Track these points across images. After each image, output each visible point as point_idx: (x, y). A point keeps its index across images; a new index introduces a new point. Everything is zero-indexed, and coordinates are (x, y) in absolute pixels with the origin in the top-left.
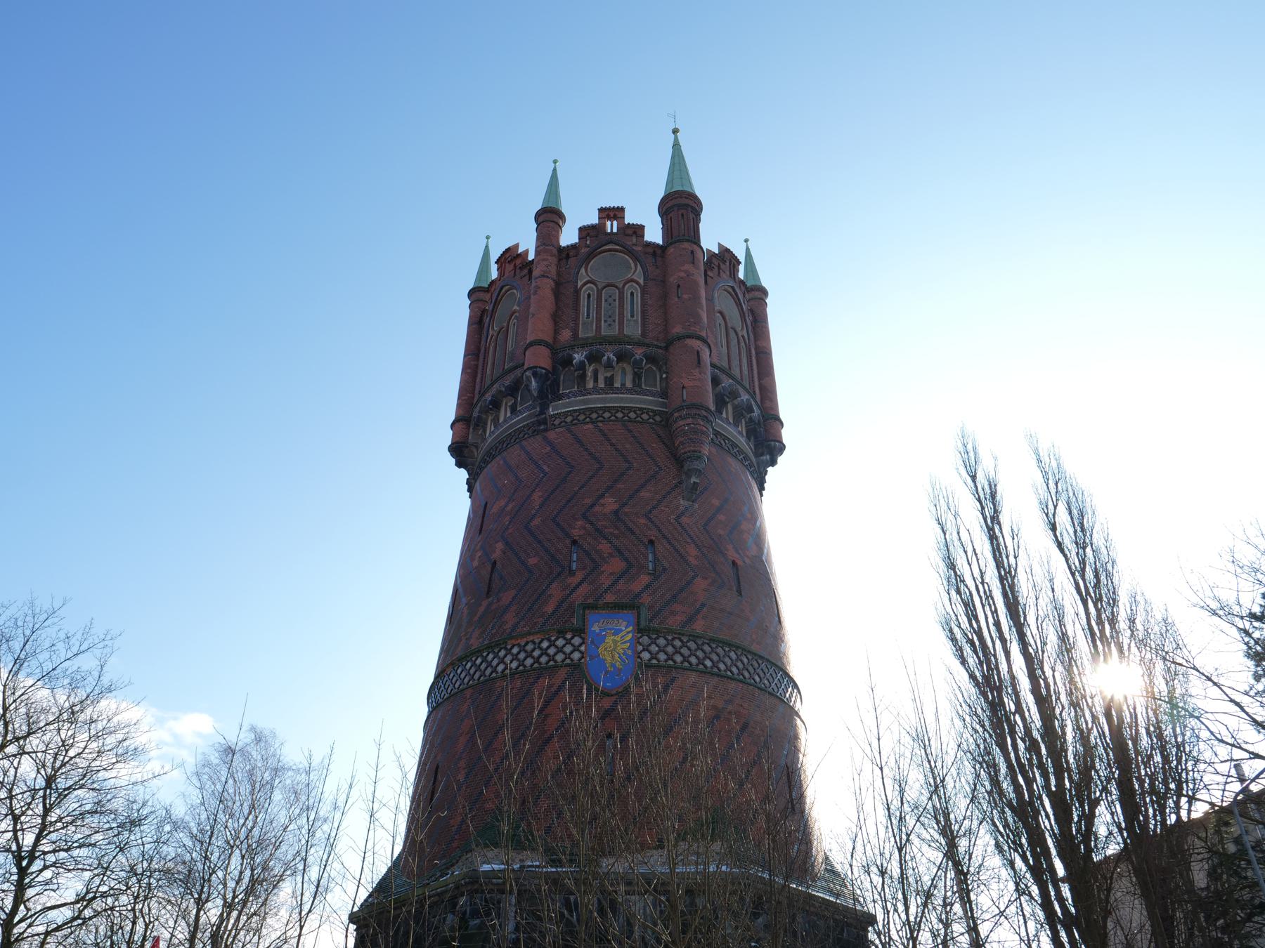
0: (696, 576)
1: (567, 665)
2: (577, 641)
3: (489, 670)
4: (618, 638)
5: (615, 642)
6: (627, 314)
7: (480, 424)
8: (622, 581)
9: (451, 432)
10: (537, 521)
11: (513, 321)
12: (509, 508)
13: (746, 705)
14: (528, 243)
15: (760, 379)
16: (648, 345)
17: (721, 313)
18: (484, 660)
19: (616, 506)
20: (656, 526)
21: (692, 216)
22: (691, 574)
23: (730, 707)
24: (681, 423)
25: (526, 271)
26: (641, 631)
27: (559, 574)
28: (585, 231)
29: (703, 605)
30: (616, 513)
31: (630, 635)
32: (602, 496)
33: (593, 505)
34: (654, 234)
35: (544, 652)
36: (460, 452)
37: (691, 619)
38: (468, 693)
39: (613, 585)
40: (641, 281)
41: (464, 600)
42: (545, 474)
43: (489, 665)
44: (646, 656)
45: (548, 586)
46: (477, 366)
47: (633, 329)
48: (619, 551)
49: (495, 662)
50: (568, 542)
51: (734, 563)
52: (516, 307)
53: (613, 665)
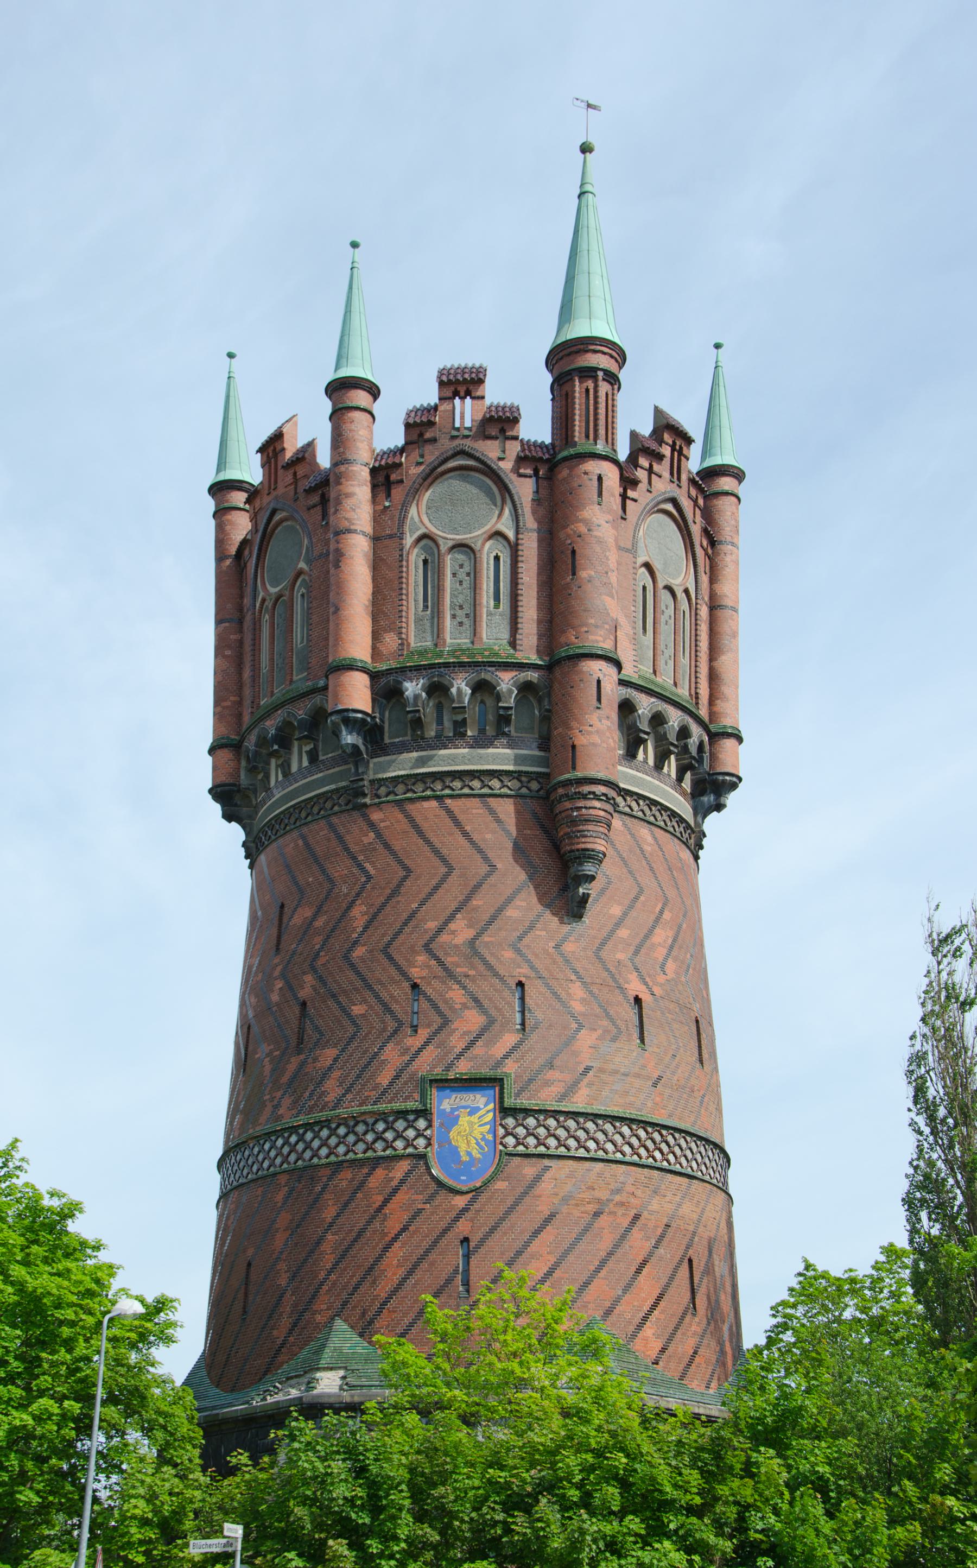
0: (581, 1026)
1: (410, 1155)
2: (421, 1124)
3: (308, 1154)
4: (474, 1118)
5: (471, 1124)
6: (486, 599)
7: (257, 766)
8: (480, 1043)
9: (217, 1177)
10: (359, 952)
11: (299, 590)
12: (319, 923)
13: (638, 1193)
14: (312, 428)
15: (712, 658)
16: (521, 666)
17: (647, 566)
18: (301, 1138)
19: (470, 933)
20: (528, 961)
21: (604, 387)
22: (574, 1026)
23: (617, 1198)
24: (568, 805)
25: (316, 499)
26: (505, 1111)
27: (395, 1032)
28: (419, 427)
29: (588, 1069)
30: (472, 942)
31: (491, 1115)
32: (452, 917)
33: (440, 930)
34: (537, 427)
35: (379, 1137)
36: (230, 798)
37: (572, 1089)
38: (283, 1179)
39: (467, 1048)
40: (511, 534)
41: (264, 1048)
42: (369, 877)
43: (308, 1146)
44: (510, 1141)
45: (381, 1048)
46: (241, 642)
47: (493, 634)
48: (476, 1000)
49: (316, 1144)
50: (406, 985)
51: (638, 1000)
52: (302, 565)
53: (469, 1154)
